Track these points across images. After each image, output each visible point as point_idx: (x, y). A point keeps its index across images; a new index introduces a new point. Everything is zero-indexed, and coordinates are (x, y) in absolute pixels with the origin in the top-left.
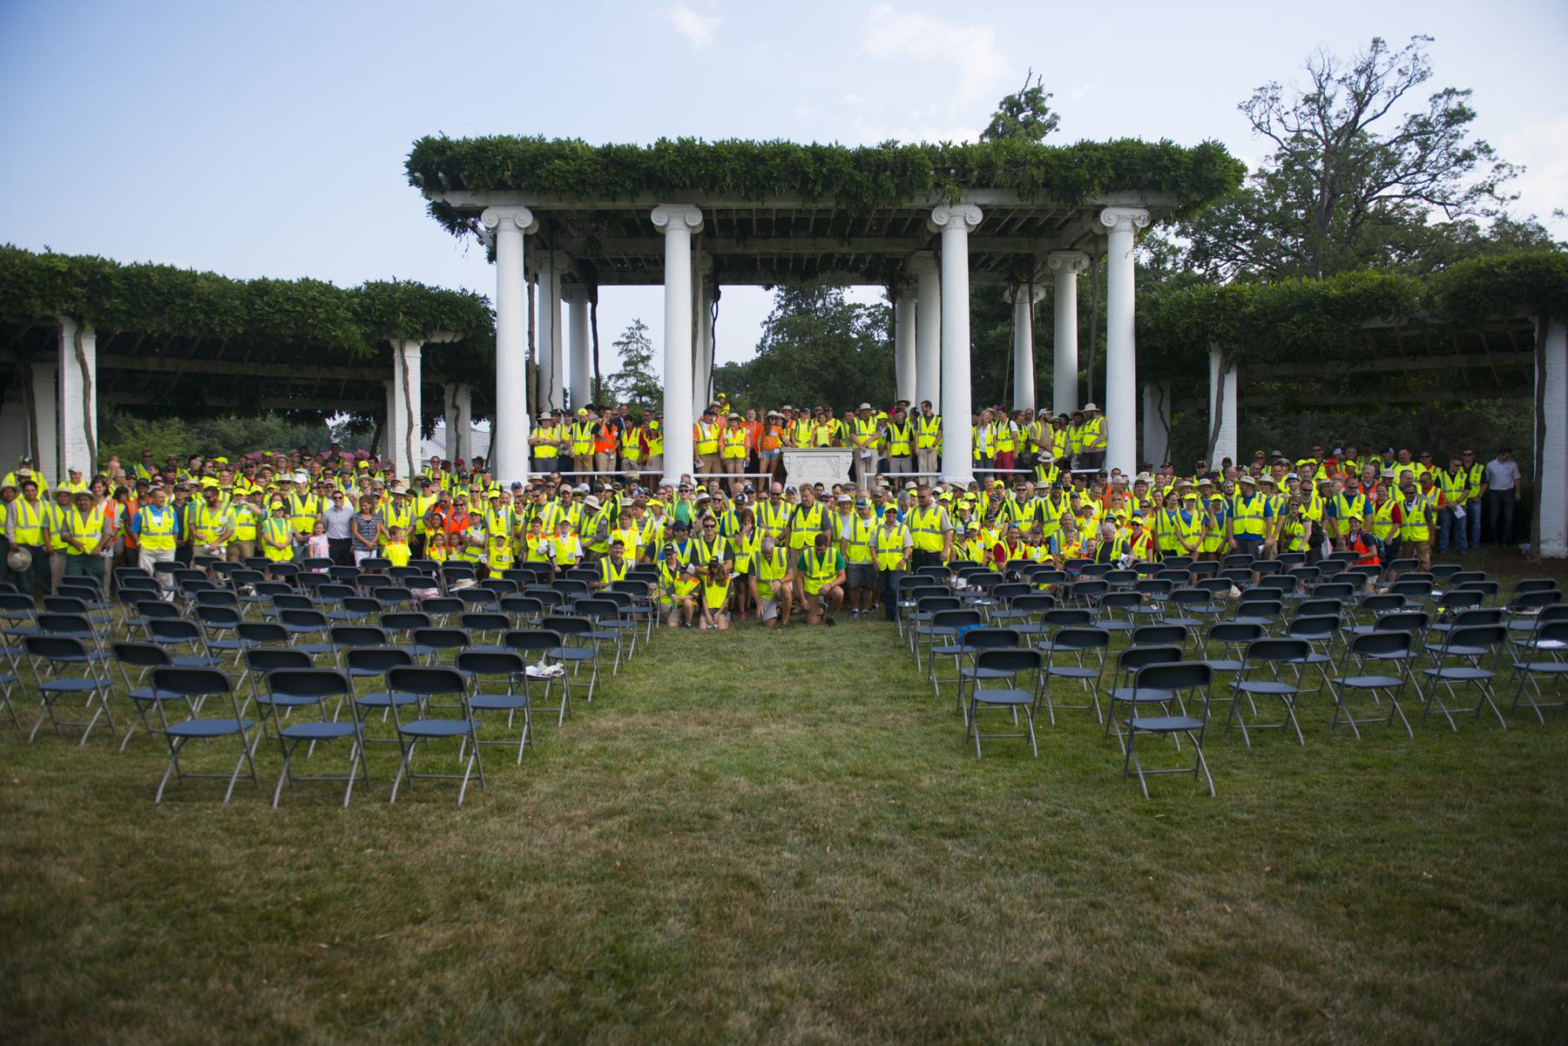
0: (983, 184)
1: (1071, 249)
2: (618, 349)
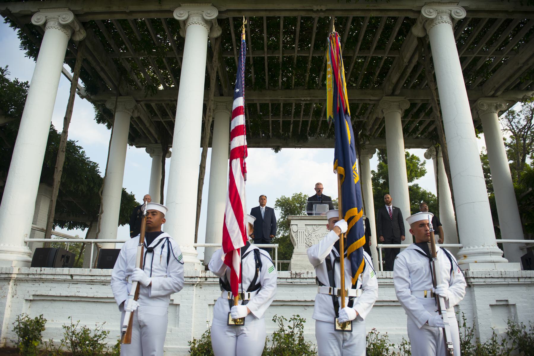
1: (493, 96)
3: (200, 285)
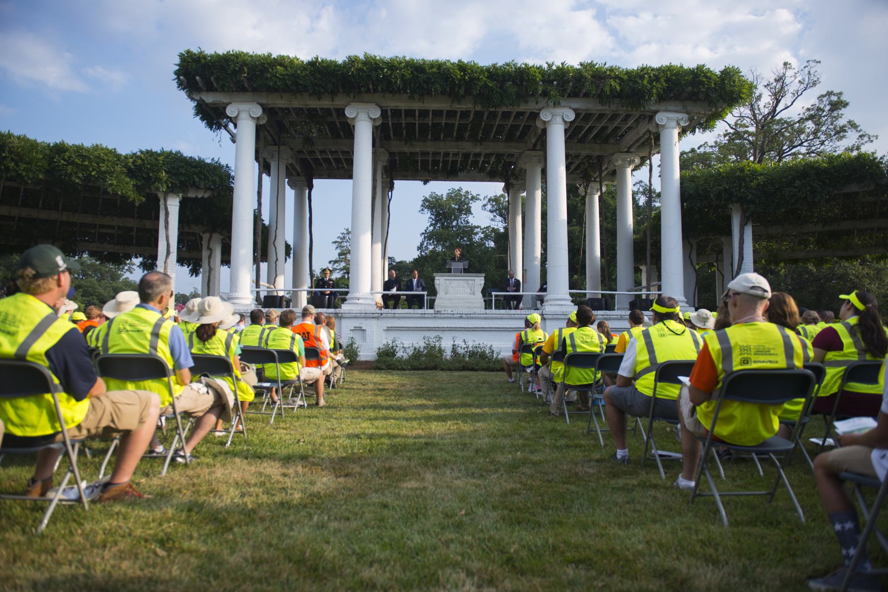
0: (574, 95)
1: (628, 152)
2: (335, 246)
3: (377, 318)
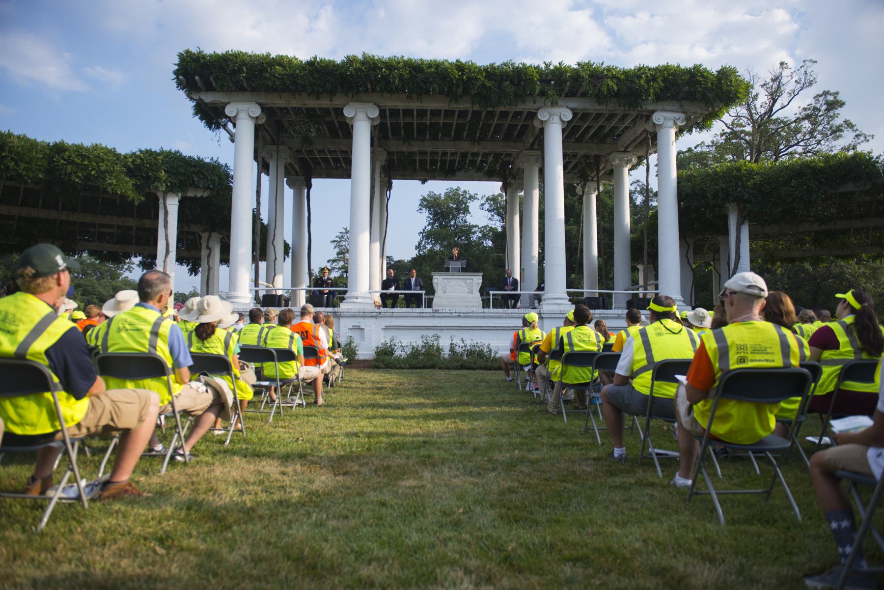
0: (572, 94)
1: (625, 151)
2: (333, 245)
3: (376, 317)
